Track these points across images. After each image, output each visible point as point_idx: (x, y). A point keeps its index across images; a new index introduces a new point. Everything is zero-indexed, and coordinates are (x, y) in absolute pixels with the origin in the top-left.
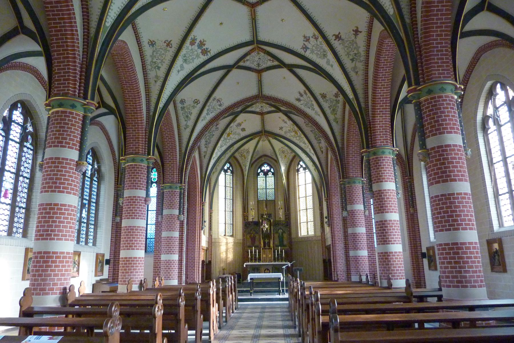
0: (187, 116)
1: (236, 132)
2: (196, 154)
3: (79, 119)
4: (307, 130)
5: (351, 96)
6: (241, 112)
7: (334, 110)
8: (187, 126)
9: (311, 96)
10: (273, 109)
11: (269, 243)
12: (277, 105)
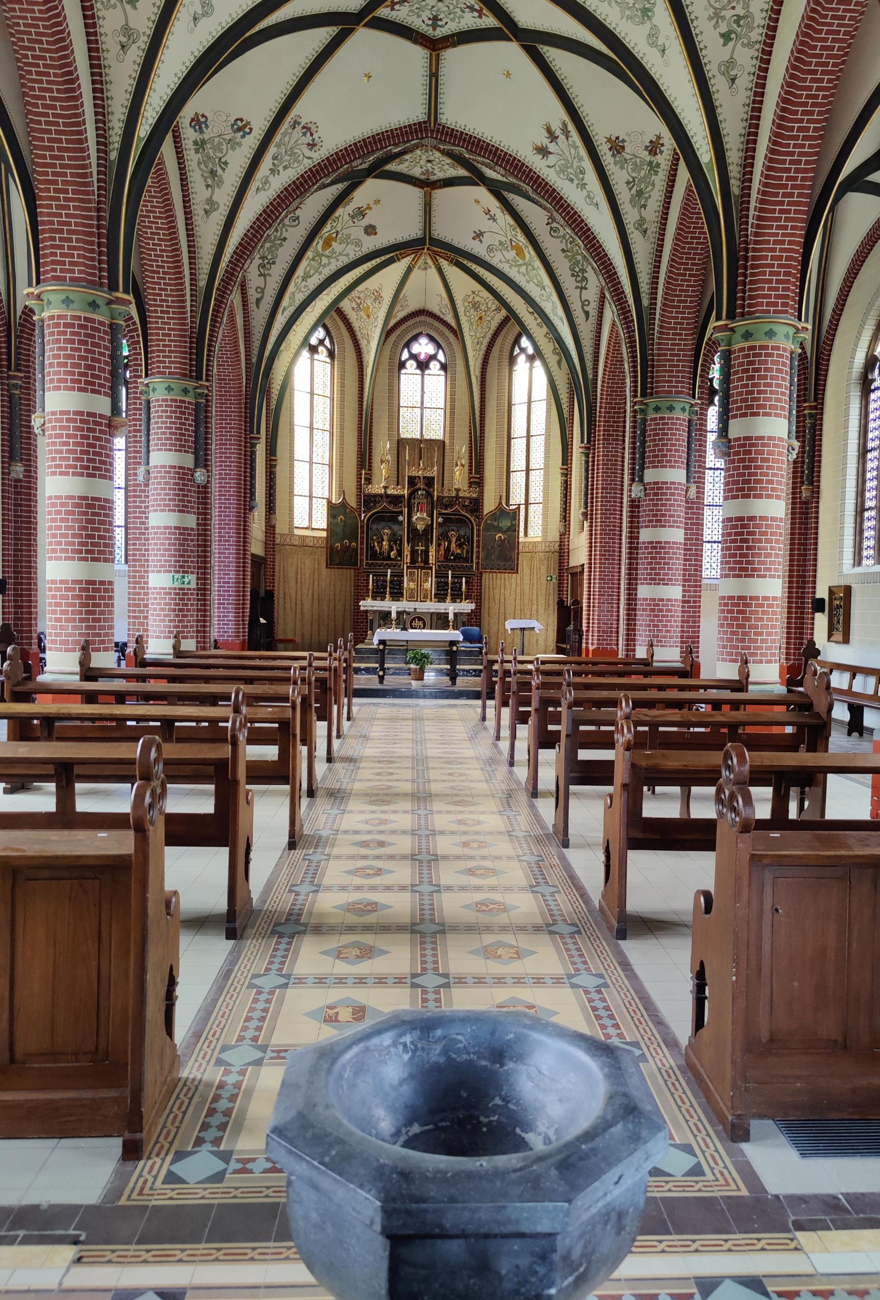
0: (213, 173)
1: (349, 236)
2: (235, 298)
4: (552, 246)
5: (705, 154)
7: (640, 193)
8: (211, 206)
9: (579, 142)
10: (462, 172)
11: (426, 552)
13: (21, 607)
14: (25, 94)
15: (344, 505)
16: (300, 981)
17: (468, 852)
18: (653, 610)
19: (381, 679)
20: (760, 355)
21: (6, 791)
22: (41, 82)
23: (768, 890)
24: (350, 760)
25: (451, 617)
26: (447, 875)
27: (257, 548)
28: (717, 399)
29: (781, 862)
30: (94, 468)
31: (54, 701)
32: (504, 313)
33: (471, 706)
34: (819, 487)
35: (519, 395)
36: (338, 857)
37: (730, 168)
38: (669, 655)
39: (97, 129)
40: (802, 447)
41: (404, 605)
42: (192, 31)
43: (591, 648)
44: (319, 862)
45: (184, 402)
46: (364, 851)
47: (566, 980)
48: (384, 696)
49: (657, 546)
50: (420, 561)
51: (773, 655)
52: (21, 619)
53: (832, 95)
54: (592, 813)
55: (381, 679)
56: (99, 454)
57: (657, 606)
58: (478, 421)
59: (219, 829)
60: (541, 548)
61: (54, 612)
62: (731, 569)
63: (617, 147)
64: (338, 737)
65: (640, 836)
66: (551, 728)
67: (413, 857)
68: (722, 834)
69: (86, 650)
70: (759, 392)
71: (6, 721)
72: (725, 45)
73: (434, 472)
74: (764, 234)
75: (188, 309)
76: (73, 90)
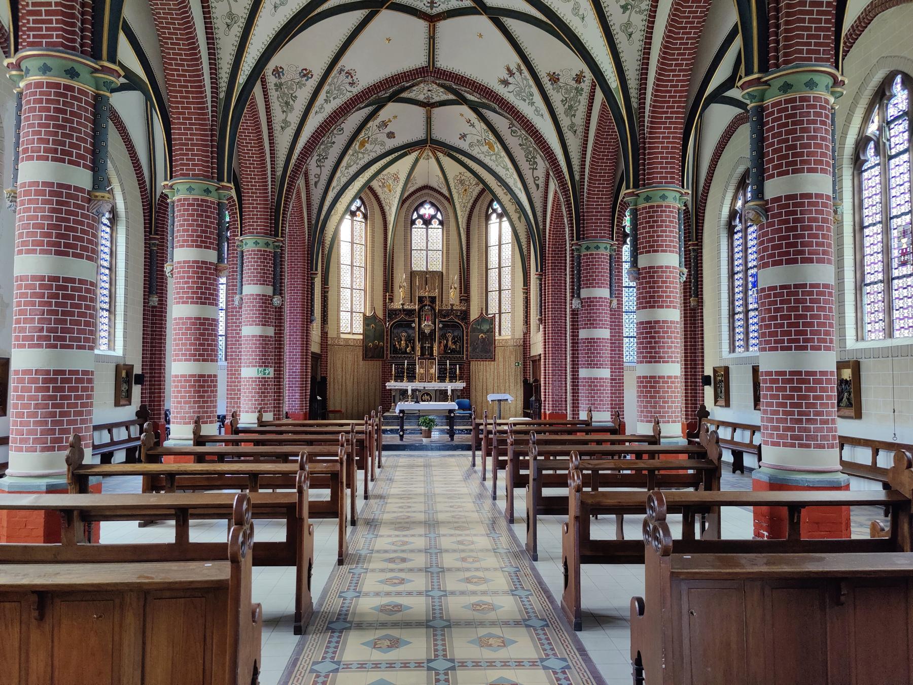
0: (287, 103)
2: (301, 182)
3: (87, 102)
4: (513, 142)
5: (613, 82)
6: (390, 99)
7: (571, 107)
8: (286, 123)
9: (529, 76)
10: (451, 97)
11: (431, 348)
12: (461, 89)
13: (154, 393)
14: (163, 57)
15: (374, 317)
16: (348, 666)
17: (465, 565)
18: (590, 386)
19: (402, 437)
20: (657, 211)
21: (140, 526)
22: (178, 70)
23: (685, 598)
24: (381, 497)
25: (449, 393)
26: (451, 583)
27: (315, 348)
28: (628, 240)
29: (693, 577)
30: (205, 298)
31: (175, 462)
32: (481, 186)
33: (464, 456)
34: (702, 298)
35: (493, 239)
36: (373, 571)
37: (631, 91)
38: (603, 417)
39: (211, 78)
40: (689, 271)
41: (417, 385)
42: (273, 15)
43: (548, 412)
44: (360, 574)
45: (266, 251)
46: (392, 566)
47: (539, 663)
48: (404, 450)
49: (591, 341)
50: (427, 354)
51: (677, 417)
52: (154, 401)
53: (697, 42)
54: (553, 533)
55: (402, 437)
56: (209, 289)
57: (593, 383)
58: (465, 252)
59: (290, 553)
60: (511, 343)
61: (176, 397)
62: (644, 357)
63: (554, 79)
64: (372, 480)
65: (588, 553)
66: (522, 472)
67: (426, 570)
68: (649, 553)
69: (197, 423)
70: (658, 236)
71: (141, 477)
72: (624, 13)
73: (436, 293)
74: (656, 133)
75: (270, 190)
76: (196, 54)
